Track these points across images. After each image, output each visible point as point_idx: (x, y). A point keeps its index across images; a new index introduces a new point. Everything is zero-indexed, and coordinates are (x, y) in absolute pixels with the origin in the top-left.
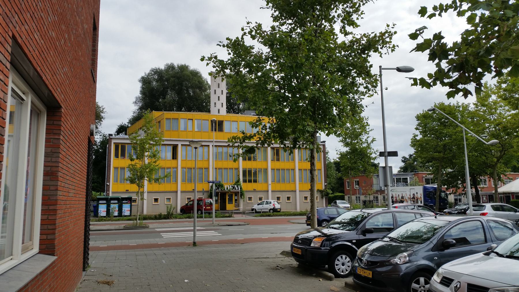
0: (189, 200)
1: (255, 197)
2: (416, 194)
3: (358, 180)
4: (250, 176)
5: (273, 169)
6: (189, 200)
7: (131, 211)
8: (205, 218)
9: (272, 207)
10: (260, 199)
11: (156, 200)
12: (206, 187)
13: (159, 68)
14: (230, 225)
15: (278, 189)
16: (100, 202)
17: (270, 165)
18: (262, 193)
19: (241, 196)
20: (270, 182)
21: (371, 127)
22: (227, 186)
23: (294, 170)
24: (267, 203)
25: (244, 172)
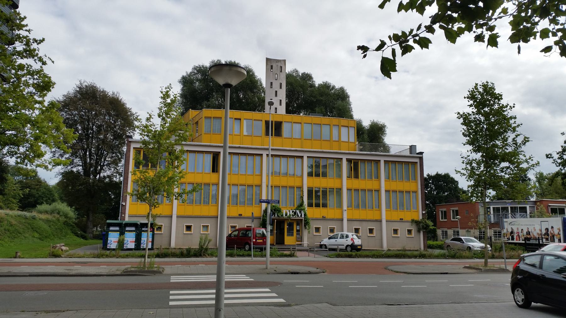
0: (233, 229)
1: (325, 227)
2: (550, 229)
3: (457, 209)
4: (318, 198)
5: (349, 190)
6: (233, 229)
7: (153, 242)
8: (255, 256)
9: (350, 243)
10: (332, 230)
11: (189, 228)
12: (258, 210)
13: (203, 66)
14: (295, 273)
15: (356, 217)
16: (111, 228)
17: (345, 183)
18: (334, 222)
19: (305, 226)
20: (345, 207)
21: (518, 121)
22: (287, 211)
23: (378, 191)
24: (342, 237)
25: (310, 192)
